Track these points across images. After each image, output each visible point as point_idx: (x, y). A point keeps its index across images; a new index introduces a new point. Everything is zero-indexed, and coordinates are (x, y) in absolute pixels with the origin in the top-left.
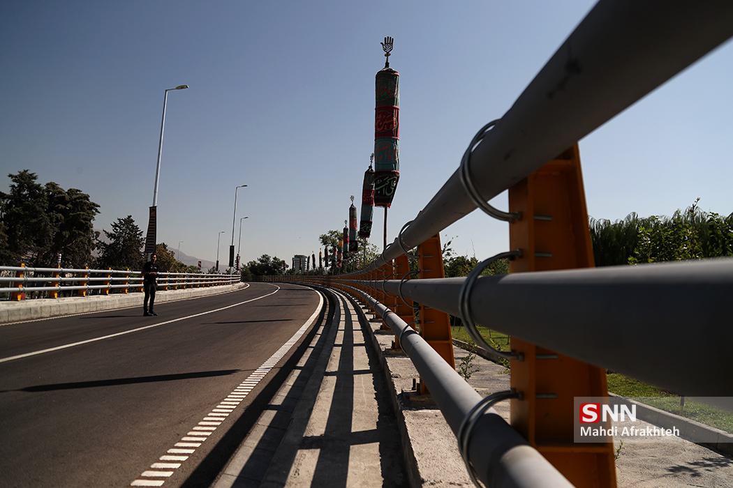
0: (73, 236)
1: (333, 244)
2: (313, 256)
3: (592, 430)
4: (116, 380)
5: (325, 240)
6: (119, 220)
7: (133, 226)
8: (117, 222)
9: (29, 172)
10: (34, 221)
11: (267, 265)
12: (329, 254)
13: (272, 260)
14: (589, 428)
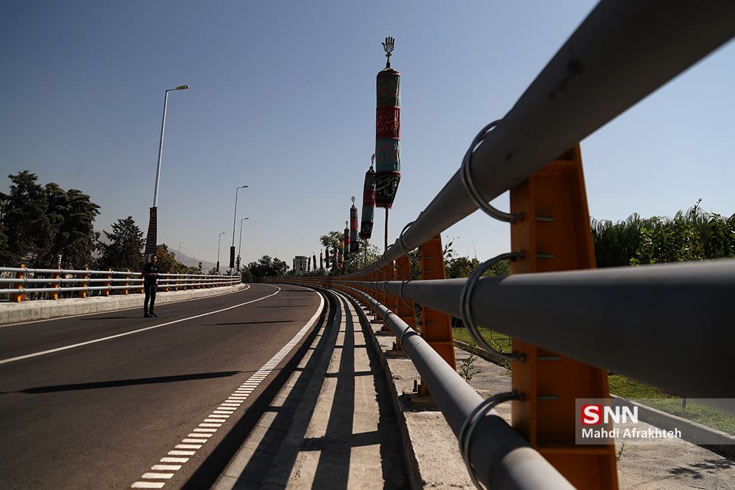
0: (73, 237)
1: (334, 245)
2: (314, 257)
3: (594, 431)
4: (117, 381)
5: (326, 241)
6: (120, 220)
7: (133, 227)
8: (118, 223)
9: (30, 173)
10: (34, 221)
11: (268, 266)
12: (330, 255)
13: (272, 261)
14: (591, 430)
